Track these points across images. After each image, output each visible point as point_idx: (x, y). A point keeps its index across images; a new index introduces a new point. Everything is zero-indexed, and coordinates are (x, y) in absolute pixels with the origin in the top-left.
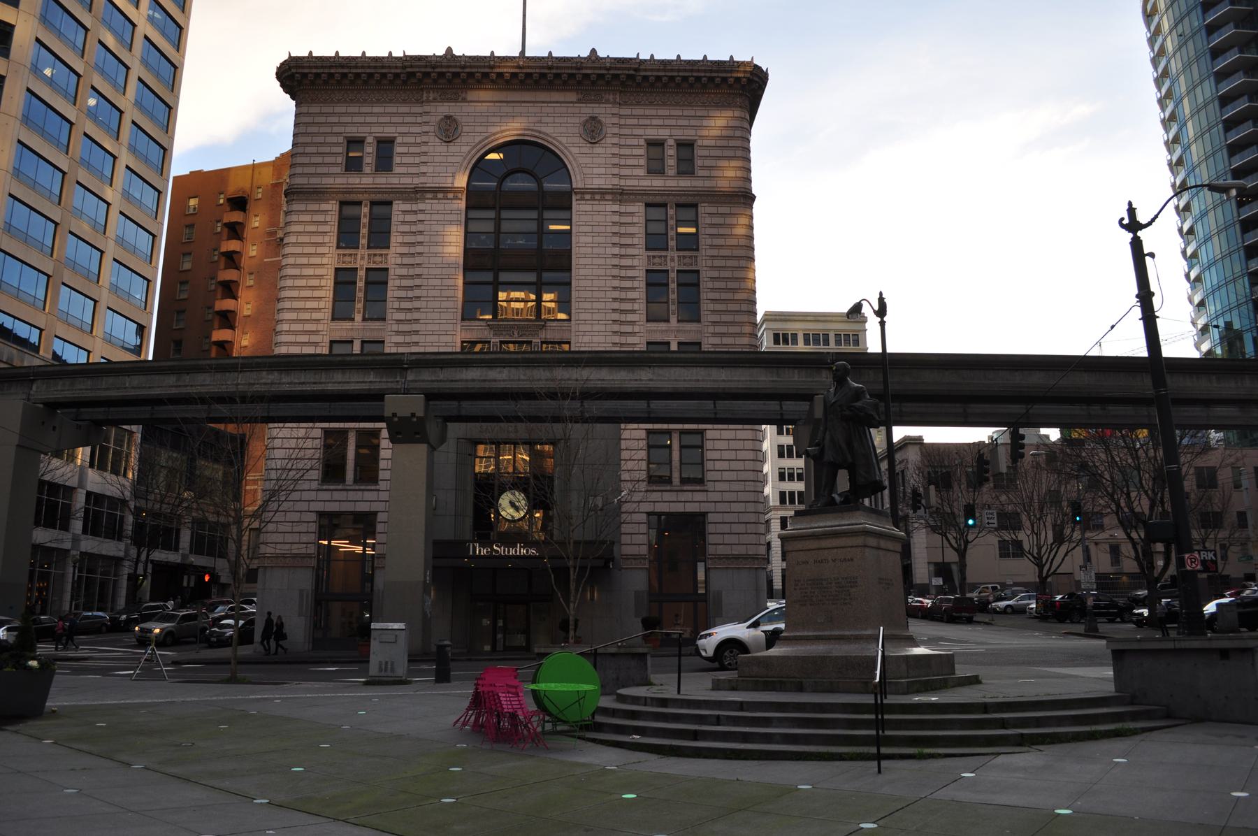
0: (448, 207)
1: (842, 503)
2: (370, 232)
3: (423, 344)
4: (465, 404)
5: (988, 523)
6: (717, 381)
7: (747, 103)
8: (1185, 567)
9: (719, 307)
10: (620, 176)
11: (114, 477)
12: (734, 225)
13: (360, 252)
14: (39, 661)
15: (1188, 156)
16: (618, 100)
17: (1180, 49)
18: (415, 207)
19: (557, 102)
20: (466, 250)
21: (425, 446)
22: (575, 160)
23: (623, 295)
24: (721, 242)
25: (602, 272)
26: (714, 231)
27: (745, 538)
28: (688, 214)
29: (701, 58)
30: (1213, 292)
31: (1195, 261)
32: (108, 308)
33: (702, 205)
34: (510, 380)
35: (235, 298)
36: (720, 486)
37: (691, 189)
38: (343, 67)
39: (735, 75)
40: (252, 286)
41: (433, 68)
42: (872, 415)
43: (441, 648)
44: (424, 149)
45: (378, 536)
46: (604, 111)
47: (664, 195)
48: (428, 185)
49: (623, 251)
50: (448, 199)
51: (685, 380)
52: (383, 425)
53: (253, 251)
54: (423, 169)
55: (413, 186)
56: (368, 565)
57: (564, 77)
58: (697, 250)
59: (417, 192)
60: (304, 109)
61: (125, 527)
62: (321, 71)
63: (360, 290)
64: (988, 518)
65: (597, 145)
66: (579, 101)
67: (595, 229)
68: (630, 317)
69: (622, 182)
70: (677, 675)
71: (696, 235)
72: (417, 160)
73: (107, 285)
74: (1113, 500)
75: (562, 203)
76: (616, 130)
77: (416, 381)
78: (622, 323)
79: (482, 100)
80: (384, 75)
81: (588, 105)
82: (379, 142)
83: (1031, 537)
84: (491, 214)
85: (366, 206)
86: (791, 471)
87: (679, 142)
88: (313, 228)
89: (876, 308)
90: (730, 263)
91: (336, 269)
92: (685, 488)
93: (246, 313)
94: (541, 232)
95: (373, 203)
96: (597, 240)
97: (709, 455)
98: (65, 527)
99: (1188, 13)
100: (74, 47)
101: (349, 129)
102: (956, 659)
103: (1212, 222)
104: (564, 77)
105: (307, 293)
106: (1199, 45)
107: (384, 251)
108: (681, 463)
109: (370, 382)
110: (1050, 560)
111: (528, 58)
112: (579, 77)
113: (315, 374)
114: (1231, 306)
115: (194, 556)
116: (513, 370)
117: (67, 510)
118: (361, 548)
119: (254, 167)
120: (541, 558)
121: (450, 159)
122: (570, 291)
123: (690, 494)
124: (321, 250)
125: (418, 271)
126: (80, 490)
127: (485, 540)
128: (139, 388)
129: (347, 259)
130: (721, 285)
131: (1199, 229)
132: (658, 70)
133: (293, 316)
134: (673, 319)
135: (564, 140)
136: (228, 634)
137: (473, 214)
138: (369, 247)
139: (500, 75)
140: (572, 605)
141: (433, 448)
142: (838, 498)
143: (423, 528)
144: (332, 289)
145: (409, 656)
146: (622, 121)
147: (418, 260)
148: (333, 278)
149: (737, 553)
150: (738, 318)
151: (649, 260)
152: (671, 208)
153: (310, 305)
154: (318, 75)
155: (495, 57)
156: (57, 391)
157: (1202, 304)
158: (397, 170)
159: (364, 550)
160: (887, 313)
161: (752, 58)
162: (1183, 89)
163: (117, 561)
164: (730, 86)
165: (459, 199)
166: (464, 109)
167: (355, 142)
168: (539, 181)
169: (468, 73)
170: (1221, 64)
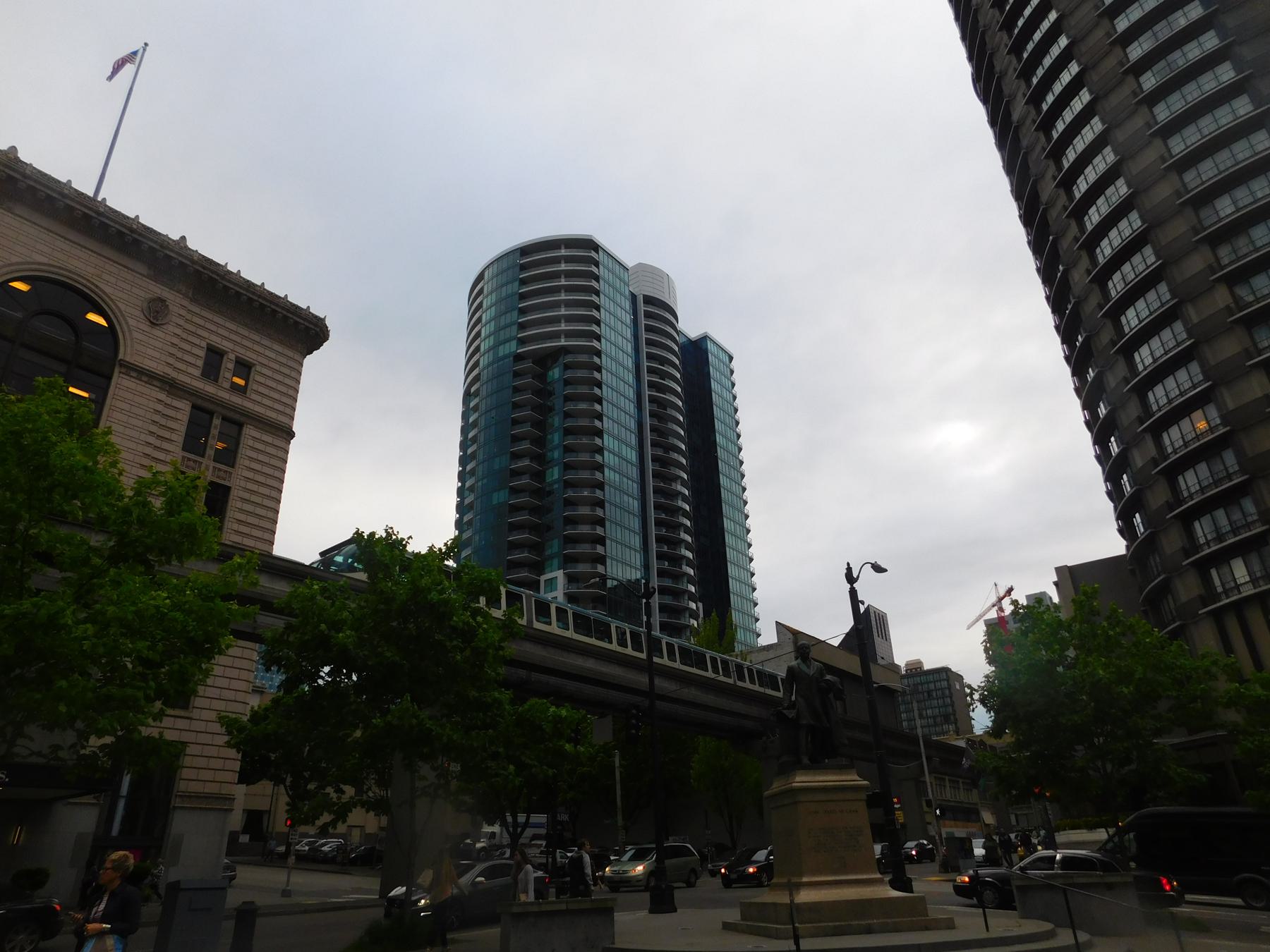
14: (969, 877)
33: (248, 426)
46: (176, 301)
58: (233, 466)
65: (158, 328)
152: (218, 418)
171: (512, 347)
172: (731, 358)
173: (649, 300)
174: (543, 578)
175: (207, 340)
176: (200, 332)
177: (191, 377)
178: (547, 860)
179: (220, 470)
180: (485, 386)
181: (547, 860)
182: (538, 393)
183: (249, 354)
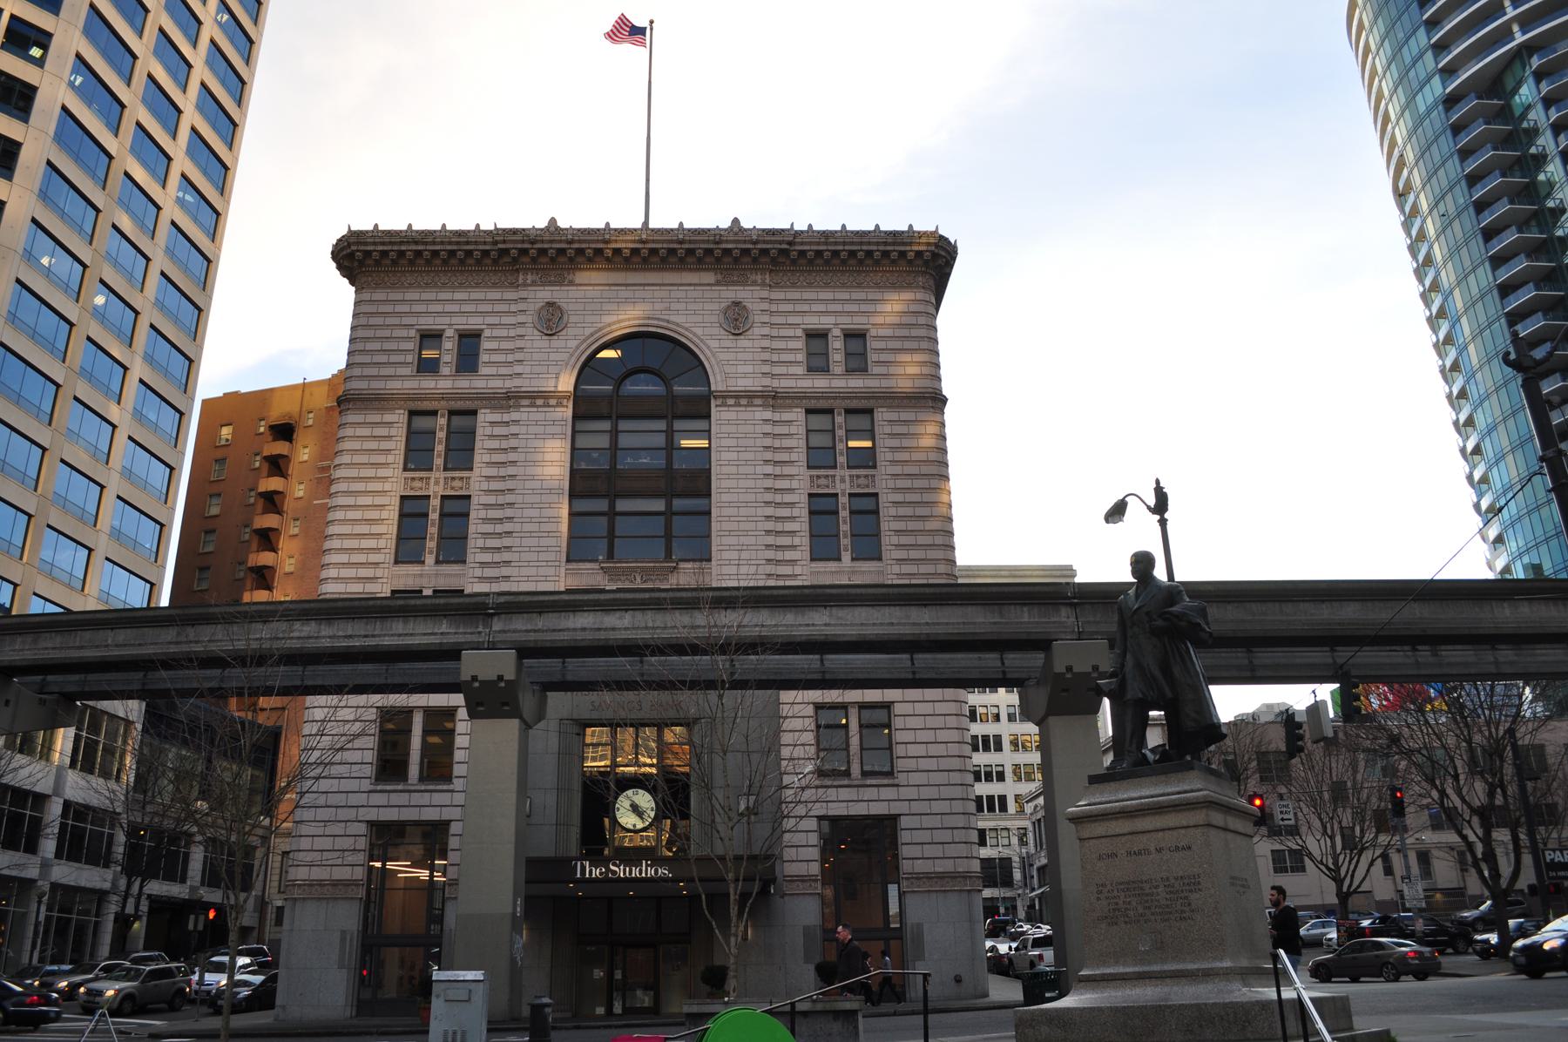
0: (550, 416)
1: (1156, 762)
2: (448, 450)
3: (516, 564)
4: (572, 663)
5: (1283, 819)
6: (919, 624)
7: (931, 282)
9: (904, 540)
11: (101, 781)
13: (434, 475)
15: (1466, 359)
16: (767, 281)
17: (1444, 231)
18: (506, 418)
19: (690, 285)
20: (574, 473)
21: (515, 722)
22: (714, 355)
23: (779, 527)
24: (904, 456)
25: (751, 497)
26: (895, 443)
27: (952, 850)
28: (861, 422)
29: (872, 228)
30: (1512, 524)
31: (1484, 487)
32: (107, 559)
33: (880, 410)
34: (634, 628)
35: (274, 550)
36: (916, 778)
38: (416, 243)
39: (916, 248)
40: (297, 535)
41: (532, 243)
43: (537, 1009)
44: (519, 344)
45: (450, 854)
46: (751, 295)
47: (829, 398)
48: (523, 389)
49: (778, 470)
50: (549, 406)
52: (457, 699)
53: (300, 491)
54: (518, 369)
55: (504, 391)
56: (438, 895)
57: (699, 253)
58: (875, 467)
59: (509, 398)
60: (366, 296)
61: (114, 848)
62: (389, 248)
63: (433, 525)
64: (1281, 812)
65: (742, 337)
66: (718, 283)
67: (741, 442)
68: (789, 555)
69: (775, 383)
71: (873, 448)
72: (510, 358)
73: (107, 529)
75: (698, 409)
76: (766, 318)
77: (504, 632)
78: (778, 562)
79: (590, 283)
80: (469, 253)
81: (730, 288)
82: (461, 336)
83: (1322, 842)
84: (606, 425)
85: (443, 416)
86: (989, 769)
88: (373, 445)
89: (1152, 502)
91: (402, 497)
92: (869, 782)
93: (288, 569)
94: (671, 447)
95: (452, 413)
96: (744, 456)
97: (899, 736)
98: (32, 848)
99: (1451, 189)
100: (81, 230)
101: (422, 320)
103: (1502, 439)
104: (699, 253)
105: (365, 529)
106: (1468, 226)
107: (465, 474)
108: (862, 749)
109: (442, 633)
110: (1350, 873)
111: (653, 230)
112: (717, 253)
113: (367, 624)
114: (1538, 541)
115: (206, 889)
116: (639, 615)
117: (36, 826)
118: (427, 873)
119: (304, 387)
120: (675, 880)
121: (553, 356)
122: (710, 521)
124: (382, 472)
125: (509, 498)
126: (55, 799)
127: (597, 858)
128: (125, 645)
129: (417, 484)
130: (908, 511)
131: (1487, 446)
132: (818, 244)
133: (344, 558)
134: (846, 557)
135: (699, 331)
136: (241, 995)
137: (581, 426)
138: (445, 469)
139: (617, 251)
140: (733, 940)
141: (527, 726)
142: (1150, 756)
143: (513, 839)
144: (396, 522)
145: (489, 1022)
146: (774, 308)
147: (510, 484)
148: (397, 508)
149: (941, 870)
150: (932, 554)
151: (812, 481)
152: (839, 414)
153: (366, 544)
154: (384, 254)
155: (610, 229)
156: (14, 651)
157: (1499, 540)
158: (483, 370)
159: (431, 876)
163: (101, 896)
164: (910, 262)
165: (563, 406)
166: (571, 294)
167: (430, 337)
168: (666, 382)
169: (577, 249)
171: (1437, 88)
176: (791, 320)
177: (799, 380)
178: (202, 977)
181: (202, 977)
182: (1508, 140)
183: (857, 319)
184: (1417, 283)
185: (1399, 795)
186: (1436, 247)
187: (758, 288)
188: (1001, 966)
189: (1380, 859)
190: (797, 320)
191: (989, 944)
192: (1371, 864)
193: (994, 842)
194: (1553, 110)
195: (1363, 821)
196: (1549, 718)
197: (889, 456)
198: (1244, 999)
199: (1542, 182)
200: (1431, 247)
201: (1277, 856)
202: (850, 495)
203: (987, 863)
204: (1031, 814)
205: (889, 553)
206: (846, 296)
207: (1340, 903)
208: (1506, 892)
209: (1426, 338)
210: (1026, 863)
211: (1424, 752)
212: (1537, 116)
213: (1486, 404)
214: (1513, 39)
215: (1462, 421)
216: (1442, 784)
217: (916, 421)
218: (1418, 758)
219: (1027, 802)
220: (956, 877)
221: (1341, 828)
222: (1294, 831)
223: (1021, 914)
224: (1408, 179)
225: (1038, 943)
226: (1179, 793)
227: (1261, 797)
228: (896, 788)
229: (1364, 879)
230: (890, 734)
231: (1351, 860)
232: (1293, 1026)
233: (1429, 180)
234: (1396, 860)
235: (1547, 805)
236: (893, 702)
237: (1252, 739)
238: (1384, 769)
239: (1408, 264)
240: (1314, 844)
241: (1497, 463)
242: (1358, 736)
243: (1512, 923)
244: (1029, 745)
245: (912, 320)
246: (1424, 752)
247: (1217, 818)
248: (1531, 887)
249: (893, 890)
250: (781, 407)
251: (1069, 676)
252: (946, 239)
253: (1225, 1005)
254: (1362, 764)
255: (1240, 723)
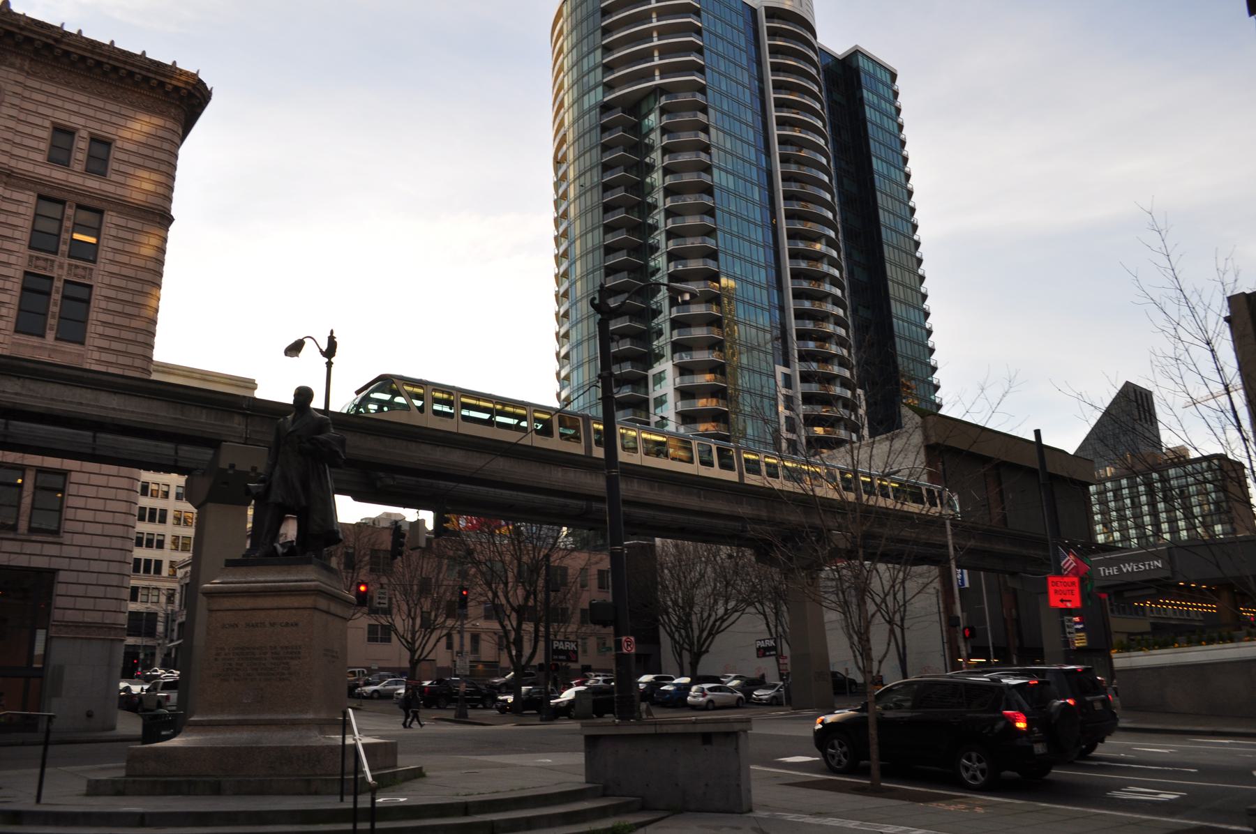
1: (284, 554)
5: (379, 603)
6: (106, 408)
8: (622, 650)
9: (109, 331)
10: (12, 156)
12: (145, 244)
16: (26, 68)
24: (125, 259)
26: (118, 245)
31: (566, 382)
33: (110, 213)
36: (79, 539)
37: (98, 192)
42: (337, 452)
51: (64, 401)
58: (94, 262)
64: (380, 598)
69: (13, 163)
70: (38, 771)
71: (96, 245)
74: (491, 588)
76: (16, 101)
83: (406, 622)
86: (151, 537)
87: (93, 136)
89: (324, 347)
90: (132, 285)
92: (34, 538)
97: (71, 501)
102: (400, 748)
106: (595, 199)
108: (33, 508)
123: (39, 545)
131: (574, 355)
132: (85, 50)
134: (50, 335)
142: (280, 549)
149: (89, 620)
150: (132, 349)
151: (30, 261)
152: (70, 207)
160: (336, 354)
161: (198, 72)
162: (578, 232)
164: (167, 93)
170: (612, 218)
171: (597, 96)
172: (894, 76)
173: (773, 13)
174: (651, 372)
175: (51, 119)
176: (42, 110)
177: (35, 163)
179: (77, 267)
180: (571, 149)
183: (107, 128)
184: (554, 228)
185: (464, 593)
186: (572, 206)
187: (15, 71)
188: (131, 703)
189: (445, 638)
190: (48, 112)
191: (123, 685)
192: (438, 641)
193: (145, 598)
194: (665, 137)
195: (438, 609)
196: (573, 550)
197: (110, 256)
198: (318, 744)
199: (648, 183)
200: (569, 206)
201: (372, 630)
202: (66, 281)
203: (134, 615)
204: (181, 579)
205: (92, 340)
206: (101, 104)
207: (411, 667)
208: (524, 668)
209: (551, 268)
210: (170, 618)
211: (489, 564)
212: (655, 137)
213: (579, 325)
214: (654, 80)
215: (561, 333)
216: (496, 588)
217: (143, 231)
218: (484, 568)
219: (179, 568)
220: (102, 627)
221: (422, 612)
222: (388, 612)
223: (158, 659)
224: (565, 153)
225: (167, 686)
226: (296, 581)
227: (366, 584)
228: (59, 546)
229: (431, 651)
230: (62, 498)
231: (425, 636)
232: (350, 763)
233: (578, 158)
234: (456, 638)
235: (562, 609)
236: (71, 471)
237: (369, 539)
238: (459, 573)
239: (551, 214)
240: (400, 622)
241: (578, 367)
242: (445, 547)
243: (524, 689)
244: (190, 521)
245: (157, 143)
246: (489, 564)
247: (323, 603)
248: (541, 665)
249: (41, 635)
250: (13, 185)
251: (231, 472)
252: (204, 84)
253: (303, 748)
254: (445, 567)
255: (360, 527)
